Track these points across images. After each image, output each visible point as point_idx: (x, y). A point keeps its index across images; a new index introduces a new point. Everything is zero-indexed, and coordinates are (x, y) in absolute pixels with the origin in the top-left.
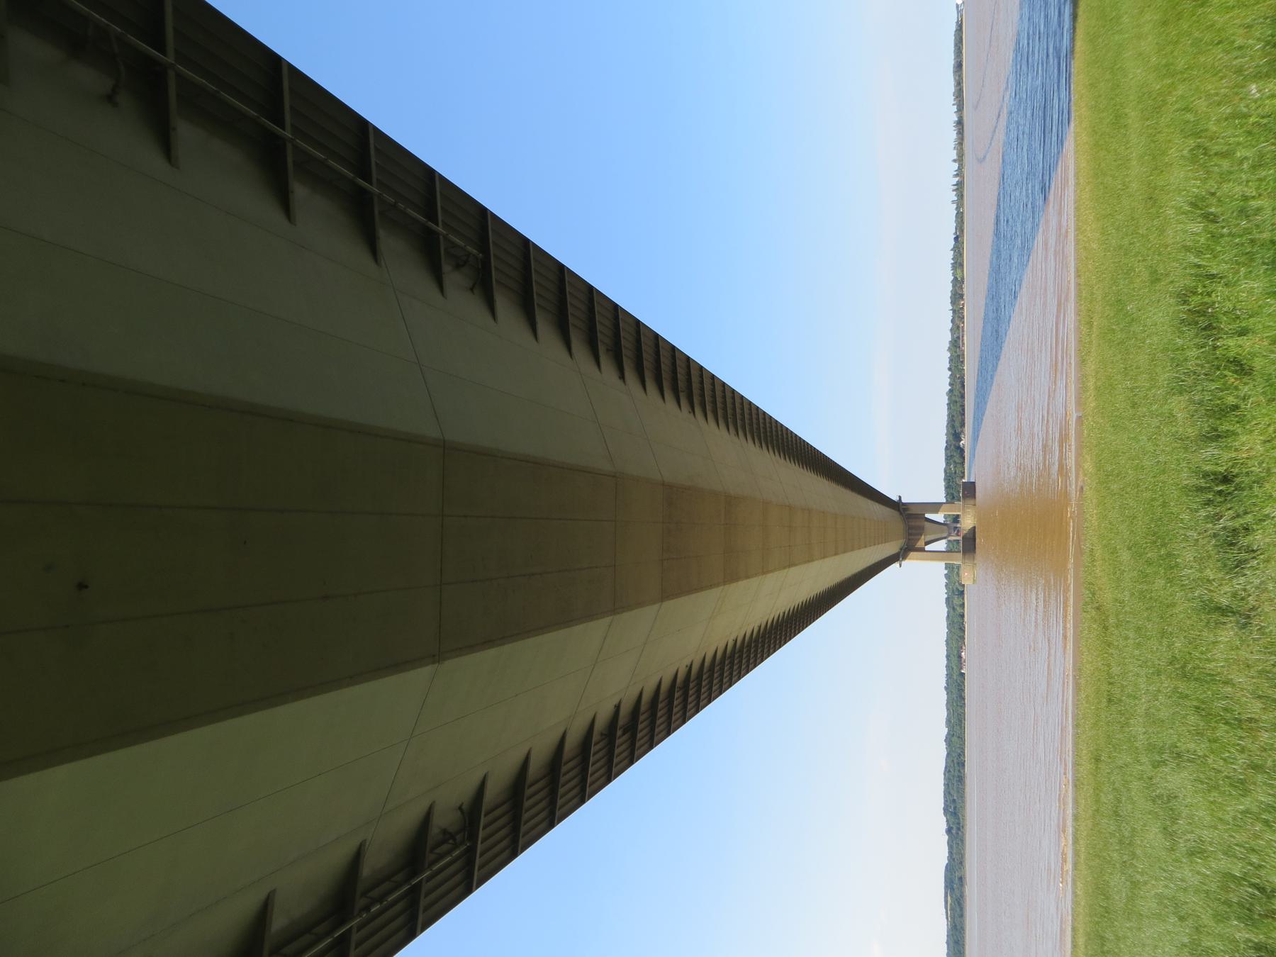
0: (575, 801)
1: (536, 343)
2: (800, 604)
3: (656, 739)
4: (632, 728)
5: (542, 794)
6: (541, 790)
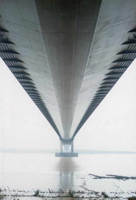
0: (8, 65)
1: (127, 32)
2: (43, 100)
3: (15, 74)
4: (24, 78)
5: (15, 71)
6: (6, 48)
